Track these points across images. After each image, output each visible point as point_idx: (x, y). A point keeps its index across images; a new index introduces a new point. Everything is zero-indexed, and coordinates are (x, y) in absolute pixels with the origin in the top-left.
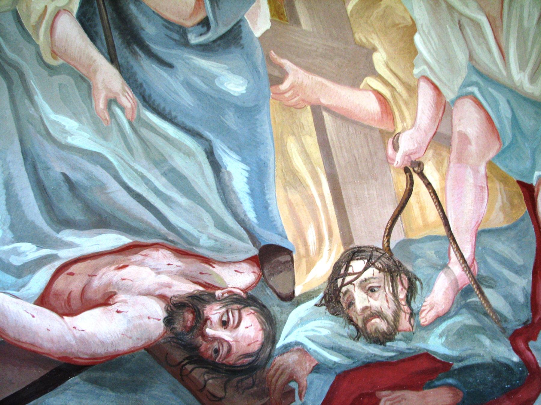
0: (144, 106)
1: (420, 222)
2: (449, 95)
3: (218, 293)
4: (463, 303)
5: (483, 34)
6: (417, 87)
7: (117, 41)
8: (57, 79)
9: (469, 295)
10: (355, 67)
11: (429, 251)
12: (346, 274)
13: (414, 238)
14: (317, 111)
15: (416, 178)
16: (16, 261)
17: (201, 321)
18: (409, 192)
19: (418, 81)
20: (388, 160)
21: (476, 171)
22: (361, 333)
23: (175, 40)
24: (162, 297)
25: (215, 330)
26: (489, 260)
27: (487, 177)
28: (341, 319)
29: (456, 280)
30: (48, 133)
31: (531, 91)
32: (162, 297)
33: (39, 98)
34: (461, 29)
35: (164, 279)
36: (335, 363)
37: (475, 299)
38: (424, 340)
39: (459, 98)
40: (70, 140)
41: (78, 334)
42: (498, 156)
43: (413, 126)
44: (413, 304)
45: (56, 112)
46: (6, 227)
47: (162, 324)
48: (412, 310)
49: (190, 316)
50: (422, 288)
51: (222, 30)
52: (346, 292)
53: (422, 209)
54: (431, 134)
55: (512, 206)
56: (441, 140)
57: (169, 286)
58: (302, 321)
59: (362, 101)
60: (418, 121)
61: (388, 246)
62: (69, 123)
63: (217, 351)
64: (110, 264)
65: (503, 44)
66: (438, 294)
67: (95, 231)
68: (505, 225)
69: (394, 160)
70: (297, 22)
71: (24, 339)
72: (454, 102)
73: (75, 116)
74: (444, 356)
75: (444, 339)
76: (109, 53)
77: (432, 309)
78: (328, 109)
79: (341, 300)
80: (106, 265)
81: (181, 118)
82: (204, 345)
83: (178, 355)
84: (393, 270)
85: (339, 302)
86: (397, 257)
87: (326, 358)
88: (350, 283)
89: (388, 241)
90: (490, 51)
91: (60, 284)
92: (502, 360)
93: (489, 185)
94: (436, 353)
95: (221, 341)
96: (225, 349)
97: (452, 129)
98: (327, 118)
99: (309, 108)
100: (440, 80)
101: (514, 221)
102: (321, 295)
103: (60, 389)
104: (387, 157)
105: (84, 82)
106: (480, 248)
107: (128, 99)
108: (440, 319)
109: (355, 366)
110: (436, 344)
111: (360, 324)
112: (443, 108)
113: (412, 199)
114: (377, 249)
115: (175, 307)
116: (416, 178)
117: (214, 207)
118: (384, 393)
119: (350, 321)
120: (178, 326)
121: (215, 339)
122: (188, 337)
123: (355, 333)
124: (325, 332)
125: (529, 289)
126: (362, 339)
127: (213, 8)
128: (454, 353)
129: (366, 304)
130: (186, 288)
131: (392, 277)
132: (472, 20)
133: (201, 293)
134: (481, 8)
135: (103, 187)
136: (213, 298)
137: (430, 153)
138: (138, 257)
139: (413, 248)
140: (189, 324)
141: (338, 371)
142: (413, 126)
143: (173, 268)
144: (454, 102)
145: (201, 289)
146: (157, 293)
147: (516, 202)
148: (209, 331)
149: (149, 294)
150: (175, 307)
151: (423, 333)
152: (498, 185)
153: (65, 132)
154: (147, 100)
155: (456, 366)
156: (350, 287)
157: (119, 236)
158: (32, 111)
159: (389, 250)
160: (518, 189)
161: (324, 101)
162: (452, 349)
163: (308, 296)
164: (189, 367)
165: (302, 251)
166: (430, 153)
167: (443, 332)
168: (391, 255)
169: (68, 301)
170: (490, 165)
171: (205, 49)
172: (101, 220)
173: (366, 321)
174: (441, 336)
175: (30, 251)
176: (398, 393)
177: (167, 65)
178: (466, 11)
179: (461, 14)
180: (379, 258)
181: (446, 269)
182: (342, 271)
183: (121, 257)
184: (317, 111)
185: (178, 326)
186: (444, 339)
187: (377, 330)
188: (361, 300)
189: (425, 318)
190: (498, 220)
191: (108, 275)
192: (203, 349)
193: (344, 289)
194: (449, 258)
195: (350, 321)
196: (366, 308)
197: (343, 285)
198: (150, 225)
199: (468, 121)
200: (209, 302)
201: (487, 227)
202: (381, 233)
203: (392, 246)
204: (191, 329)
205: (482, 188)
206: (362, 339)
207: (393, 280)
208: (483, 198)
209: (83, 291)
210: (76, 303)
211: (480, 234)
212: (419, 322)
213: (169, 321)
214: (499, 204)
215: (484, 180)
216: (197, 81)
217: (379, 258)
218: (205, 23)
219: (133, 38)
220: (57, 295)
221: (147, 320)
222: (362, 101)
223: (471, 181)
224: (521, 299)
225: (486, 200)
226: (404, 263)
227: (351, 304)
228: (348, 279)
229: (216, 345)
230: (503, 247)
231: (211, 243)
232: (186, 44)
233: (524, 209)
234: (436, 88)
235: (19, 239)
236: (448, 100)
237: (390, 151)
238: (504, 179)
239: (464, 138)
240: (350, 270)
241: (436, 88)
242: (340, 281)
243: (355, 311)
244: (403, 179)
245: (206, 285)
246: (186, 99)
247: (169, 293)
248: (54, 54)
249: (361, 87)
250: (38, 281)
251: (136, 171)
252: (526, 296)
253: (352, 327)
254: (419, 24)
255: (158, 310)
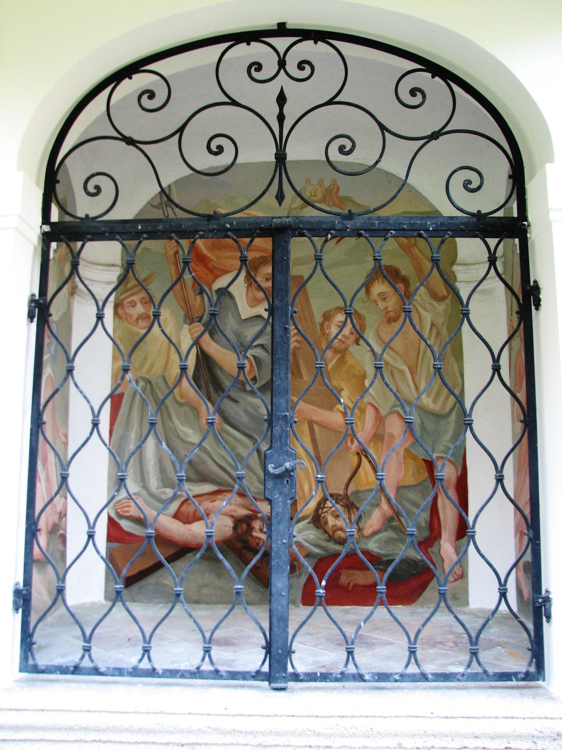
0: (224, 422)
1: (364, 480)
2: (383, 413)
3: (259, 515)
4: (389, 525)
5: (405, 377)
6: (365, 409)
7: (211, 390)
8: (183, 409)
9: (392, 521)
10: (332, 398)
11: (369, 497)
12: (324, 507)
13: (361, 489)
14: (311, 423)
15: (363, 458)
16: (164, 497)
17: (250, 528)
18: (359, 465)
19: (366, 405)
20: (348, 449)
21: (398, 454)
22: (331, 538)
23: (239, 388)
24: (232, 516)
25: (257, 533)
26: (405, 503)
27: (404, 457)
28: (321, 531)
29: (385, 512)
30: (179, 436)
31: (432, 408)
32: (232, 516)
33: (175, 419)
34: (392, 375)
35: (233, 507)
36: (317, 553)
37: (396, 523)
38: (366, 544)
39: (389, 414)
40: (189, 439)
41: (191, 533)
42: (411, 446)
43: (362, 430)
44: (360, 524)
45: (183, 425)
46: (159, 481)
47: (231, 529)
48: (359, 528)
49: (245, 526)
50: (365, 515)
51: (263, 382)
52: (324, 517)
53: (366, 474)
54: (372, 434)
55: (419, 473)
56: (378, 437)
57: (235, 511)
58: (300, 531)
59: (335, 418)
60: (365, 428)
61: (347, 494)
62: (189, 431)
63: (258, 544)
64: (208, 499)
65: (417, 383)
66: (374, 520)
67: (200, 483)
68: (414, 483)
69: (351, 449)
70: (301, 376)
71: (167, 534)
72: (386, 416)
73: (191, 427)
74: (378, 553)
75: (377, 544)
76: (208, 396)
77: (370, 527)
78: (316, 422)
79: (321, 521)
80: (205, 500)
81: (242, 428)
82: (251, 540)
83: (239, 545)
84: (350, 506)
85: (320, 522)
86: (352, 499)
87: (312, 550)
88: (326, 512)
89: (347, 491)
90: (409, 386)
91: (184, 508)
92: (411, 557)
93: (406, 462)
94: (372, 551)
95: (260, 539)
96: (262, 543)
97: (384, 431)
98: (316, 427)
99: (306, 422)
100: (379, 404)
101: (420, 481)
102: (311, 518)
103: (182, 559)
104: (347, 447)
105: (195, 410)
106: (399, 496)
107: (217, 418)
108: (375, 533)
109: (328, 555)
110: (373, 546)
111: (331, 533)
112: (380, 420)
113: (361, 469)
114: (341, 495)
115: (238, 522)
116: (363, 458)
117: (258, 472)
118: (343, 571)
119: (326, 532)
120: (239, 531)
121: (257, 538)
122: (244, 537)
123: (328, 538)
124: (312, 537)
125: (428, 519)
126: (332, 541)
127: (258, 370)
128: (383, 552)
129: (334, 523)
130: (244, 512)
131: (348, 509)
132: (399, 370)
133: (251, 515)
134: (405, 362)
135: (204, 462)
136: (256, 518)
137: (372, 444)
138: (220, 497)
139: (360, 495)
140: (245, 530)
141: (319, 557)
142: (362, 430)
143: (238, 502)
144: (386, 416)
145: (251, 513)
146: (230, 514)
147: (421, 471)
148: (254, 534)
149: (225, 514)
150: (238, 522)
151: (366, 540)
152: (411, 462)
153: (187, 435)
154: (226, 420)
155: (385, 559)
156: (326, 514)
157: (211, 486)
158: (171, 425)
159: (347, 496)
160: (423, 464)
161: (314, 418)
162: (381, 549)
163: (304, 518)
164: (244, 551)
165: (301, 495)
166: (372, 444)
167: (377, 540)
168: (348, 498)
169: (187, 517)
170: (407, 450)
171: (252, 393)
172: (203, 478)
173: (334, 532)
174: (376, 542)
175: (169, 492)
176: (351, 571)
177: (236, 401)
178: (396, 365)
179: (392, 367)
180: (342, 500)
181: (379, 507)
182: (322, 506)
183: (213, 496)
184: (311, 423)
185: (239, 531)
186: (377, 544)
187: (340, 537)
188: (331, 521)
189: (367, 531)
190: (410, 480)
191: (205, 505)
192: (251, 543)
193: (322, 515)
194: (381, 501)
195: (326, 532)
196: (334, 526)
197: (322, 513)
198: (226, 481)
199: (395, 427)
200: (254, 519)
201: (403, 485)
202: (343, 486)
203: (349, 493)
204: (246, 533)
205: (401, 463)
206: (332, 541)
207: (349, 512)
208: (401, 469)
209: (195, 512)
210: (191, 518)
211: (399, 488)
212: (363, 534)
213: (235, 528)
214: (411, 472)
215: (403, 458)
216: (250, 409)
217: (342, 500)
218: (254, 379)
219: (219, 387)
220: (182, 514)
221: (224, 527)
222: (335, 418)
223: (395, 459)
224: (423, 524)
225: (403, 470)
226: (355, 502)
227: (326, 523)
228: (325, 510)
229: (257, 541)
230: (412, 495)
231: (256, 490)
232: (245, 390)
233: (426, 475)
234: (376, 409)
235: (165, 486)
236: (383, 415)
237: (349, 444)
238: (415, 458)
239: (392, 436)
240: (326, 506)
241: (376, 409)
242: (320, 511)
243: (328, 526)
244: (355, 459)
245: (253, 511)
246: (245, 419)
247: (235, 514)
248: (182, 396)
249: (335, 410)
250: (174, 507)
251: (220, 454)
252: (426, 522)
253: (327, 535)
254: (368, 373)
255: (230, 523)
